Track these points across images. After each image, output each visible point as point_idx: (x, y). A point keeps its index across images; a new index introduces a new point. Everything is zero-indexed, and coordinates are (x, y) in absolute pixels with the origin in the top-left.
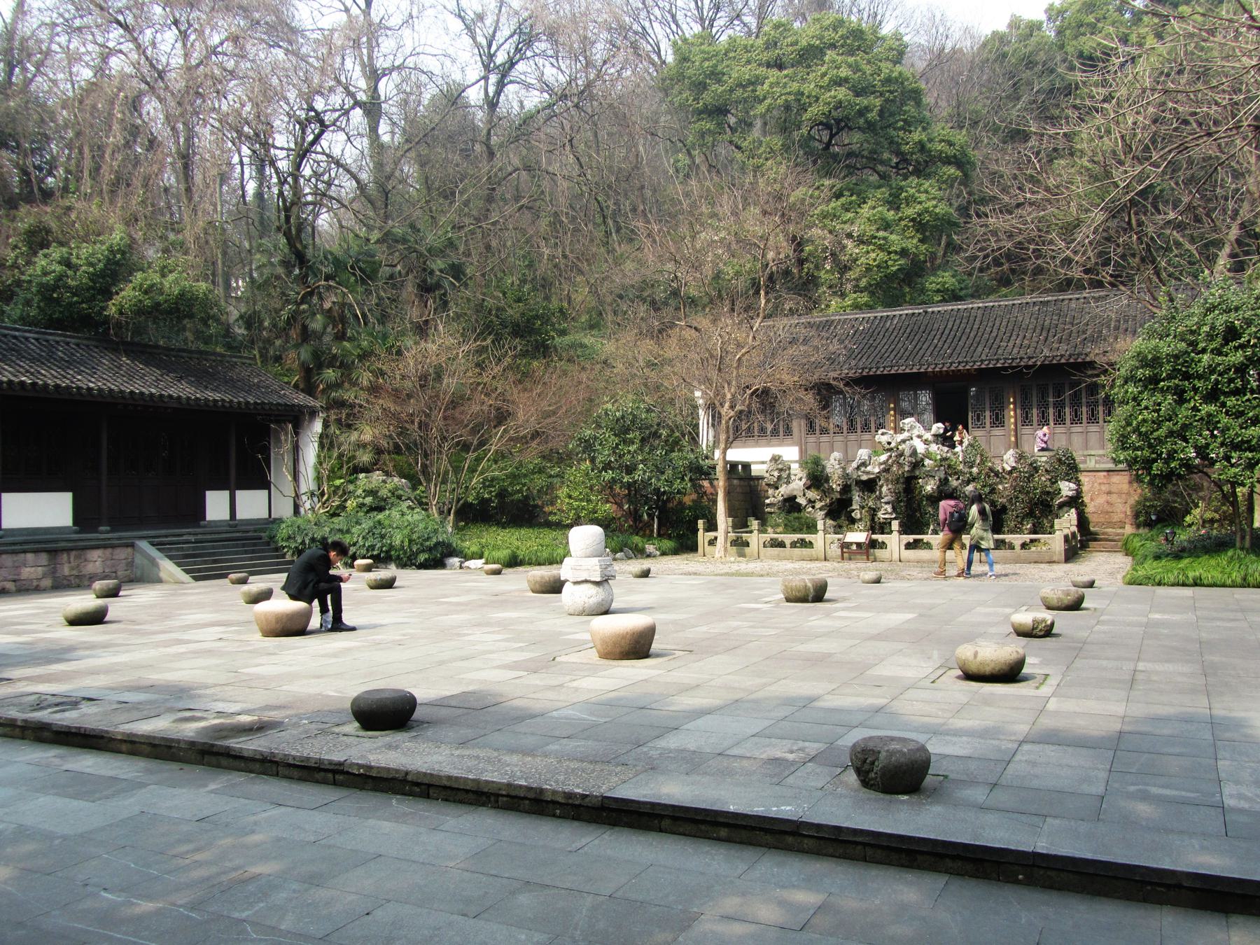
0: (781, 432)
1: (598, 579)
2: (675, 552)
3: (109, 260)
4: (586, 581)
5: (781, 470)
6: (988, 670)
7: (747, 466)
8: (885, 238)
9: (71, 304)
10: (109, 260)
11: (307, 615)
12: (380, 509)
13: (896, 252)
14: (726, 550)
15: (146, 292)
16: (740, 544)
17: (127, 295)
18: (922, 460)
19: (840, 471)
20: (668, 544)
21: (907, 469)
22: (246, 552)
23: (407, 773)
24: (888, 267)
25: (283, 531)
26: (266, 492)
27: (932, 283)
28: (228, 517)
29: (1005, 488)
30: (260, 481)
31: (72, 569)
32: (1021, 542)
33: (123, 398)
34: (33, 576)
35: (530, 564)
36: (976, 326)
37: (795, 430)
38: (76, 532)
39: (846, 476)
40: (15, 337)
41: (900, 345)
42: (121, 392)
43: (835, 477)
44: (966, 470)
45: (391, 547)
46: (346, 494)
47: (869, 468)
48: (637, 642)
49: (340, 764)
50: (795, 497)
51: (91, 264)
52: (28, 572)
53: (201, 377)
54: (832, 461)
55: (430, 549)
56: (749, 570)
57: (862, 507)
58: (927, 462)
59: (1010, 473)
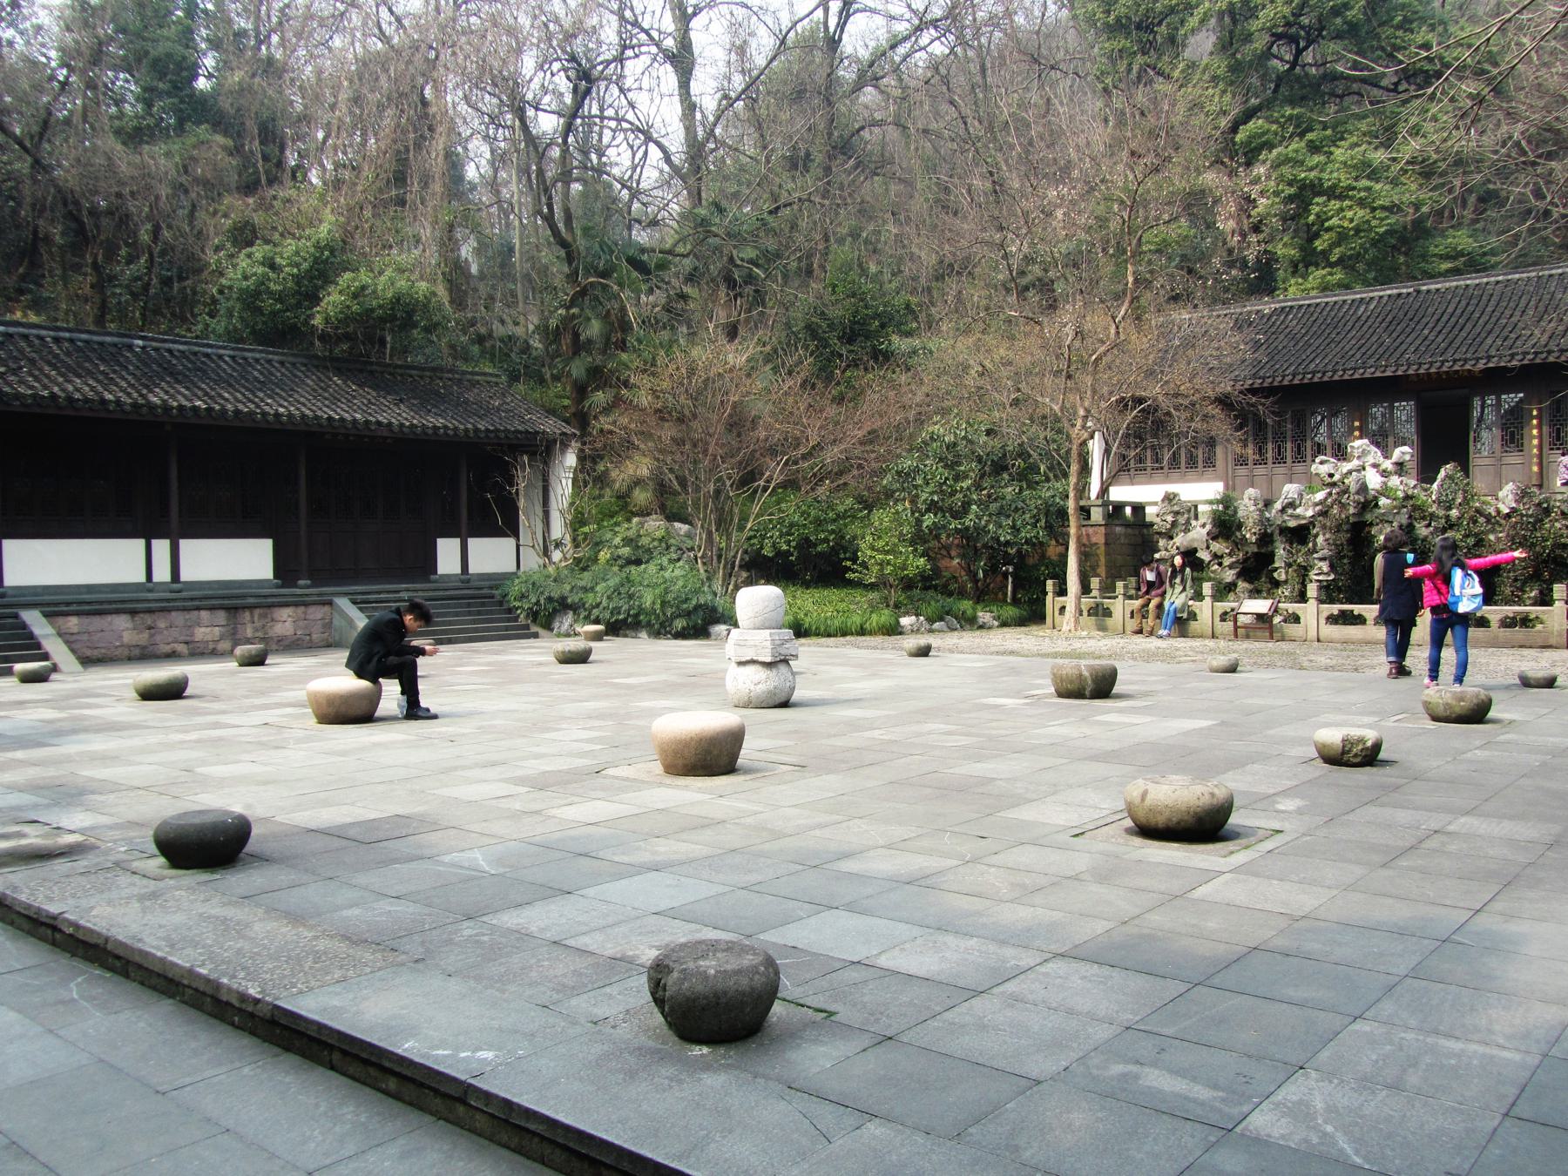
0: (1196, 459)
1: (768, 659)
2: (1021, 622)
3: (316, 259)
4: (753, 662)
5: (1177, 513)
6: (1161, 820)
7: (1139, 509)
8: (1368, 189)
9: (274, 314)
10: (316, 259)
11: (375, 697)
12: (638, 562)
13: (1383, 208)
14: (1077, 621)
15: (355, 296)
16: (1100, 613)
17: (333, 300)
18: (1376, 498)
19: (1256, 515)
20: (1011, 611)
21: (1352, 511)
22: (469, 613)
23: (107, 940)
24: (1371, 229)
25: (516, 588)
26: (511, 542)
27: (1438, 246)
28: (459, 571)
29: (1498, 539)
30: (508, 527)
31: (257, 630)
32: (1499, 617)
33: (321, 426)
34: (209, 638)
35: (817, 634)
36: (1489, 309)
37: (1220, 462)
38: (278, 587)
39: (1264, 522)
40: (207, 355)
41: (1374, 339)
42: (317, 417)
43: (1250, 523)
44: (1441, 513)
45: (641, 610)
46: (598, 545)
47: (1299, 511)
48: (708, 752)
49: (55, 918)
50: (1195, 550)
51: (297, 265)
52: (201, 633)
53: (427, 398)
54: (1246, 500)
55: (688, 614)
56: (1084, 649)
57: (1289, 565)
58: (1383, 501)
59: (1508, 516)
